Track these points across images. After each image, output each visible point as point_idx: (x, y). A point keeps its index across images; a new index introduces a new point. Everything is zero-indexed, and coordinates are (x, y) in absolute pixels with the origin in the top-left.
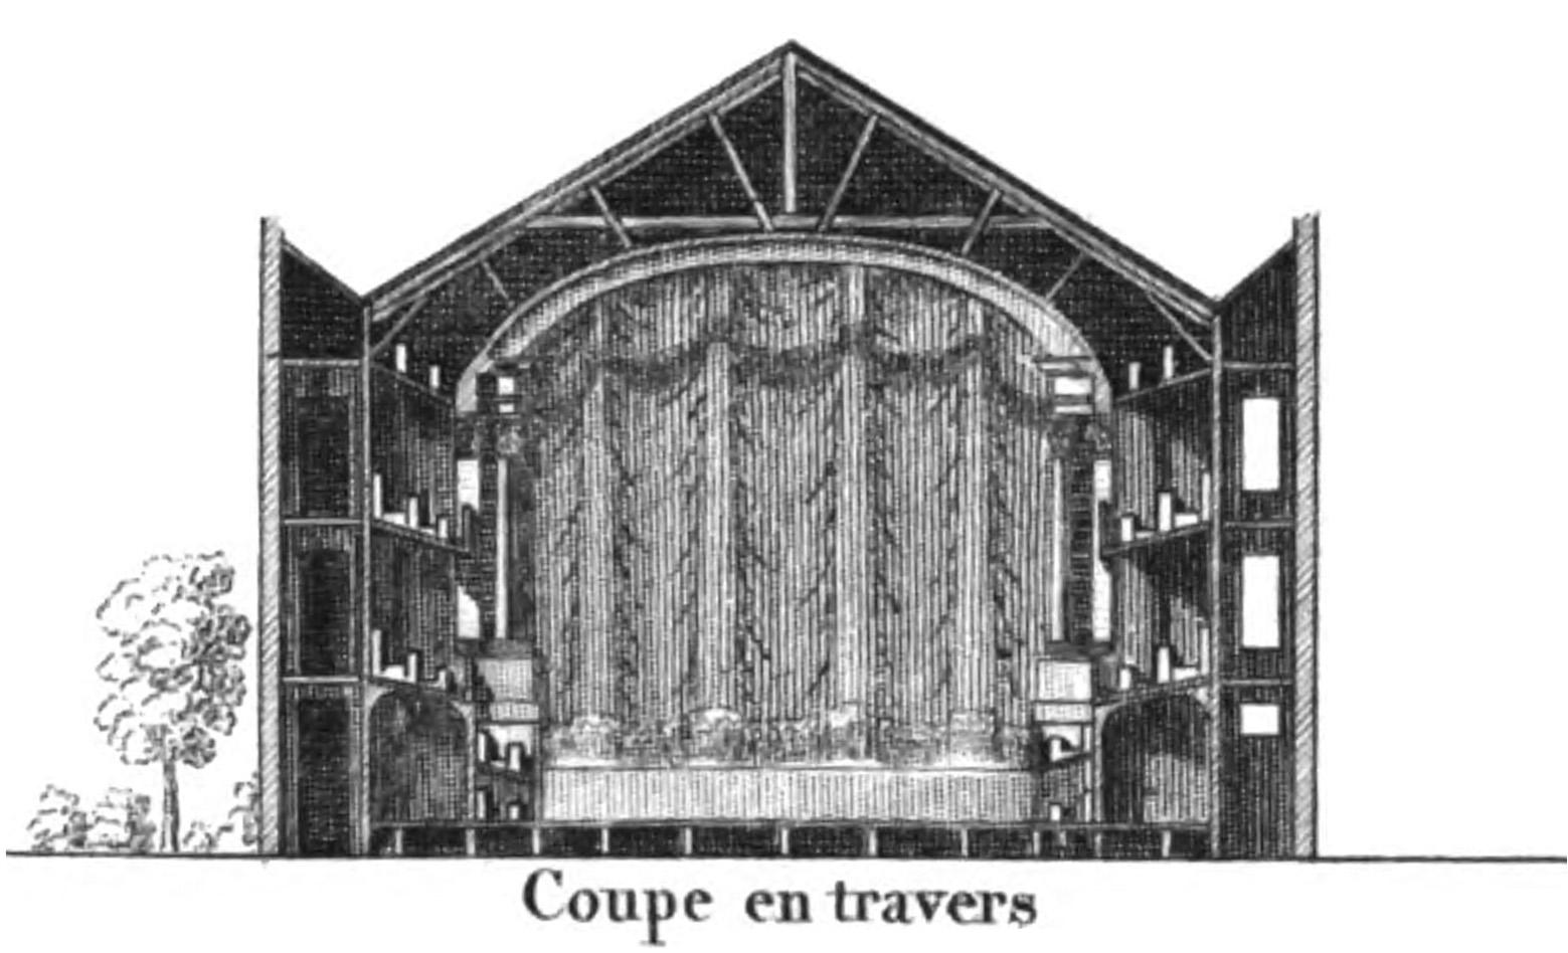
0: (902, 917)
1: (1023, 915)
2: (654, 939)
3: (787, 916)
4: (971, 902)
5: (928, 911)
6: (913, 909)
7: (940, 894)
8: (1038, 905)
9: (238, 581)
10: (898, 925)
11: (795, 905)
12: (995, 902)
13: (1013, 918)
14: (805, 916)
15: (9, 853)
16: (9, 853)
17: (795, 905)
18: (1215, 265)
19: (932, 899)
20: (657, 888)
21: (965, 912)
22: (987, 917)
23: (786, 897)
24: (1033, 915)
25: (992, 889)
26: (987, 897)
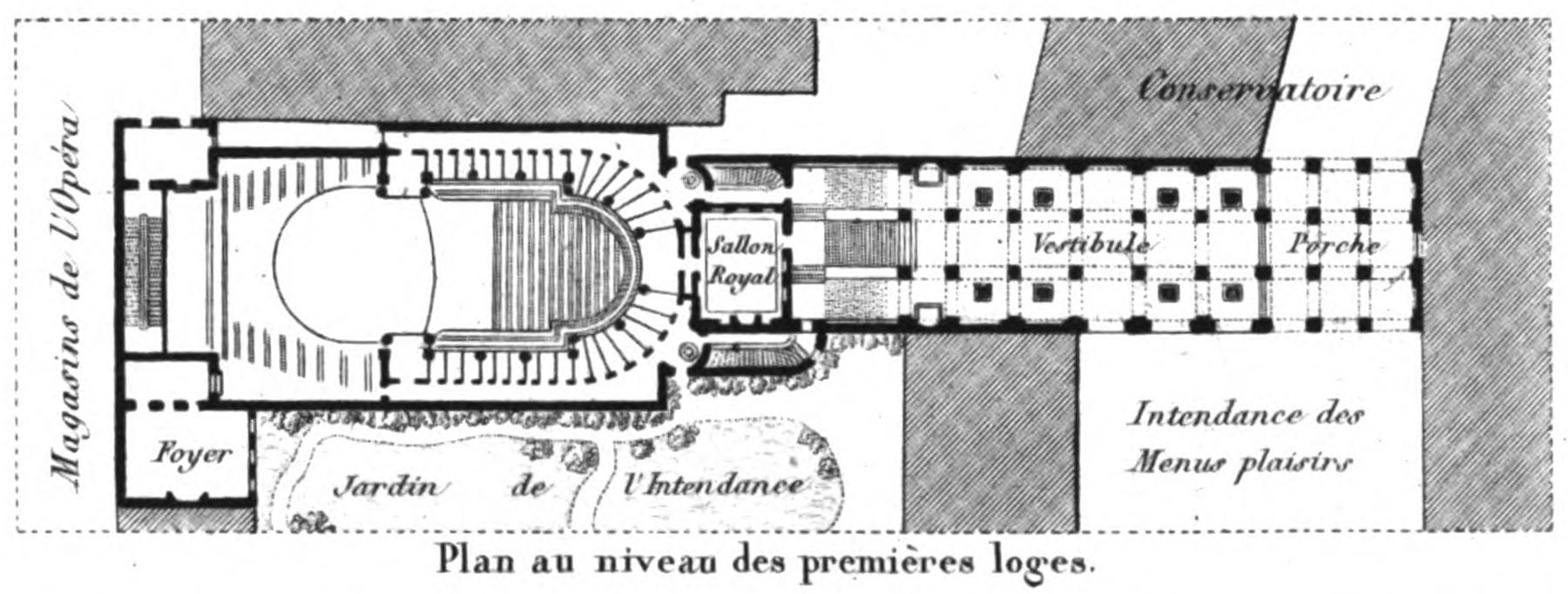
1: (1078, 568)
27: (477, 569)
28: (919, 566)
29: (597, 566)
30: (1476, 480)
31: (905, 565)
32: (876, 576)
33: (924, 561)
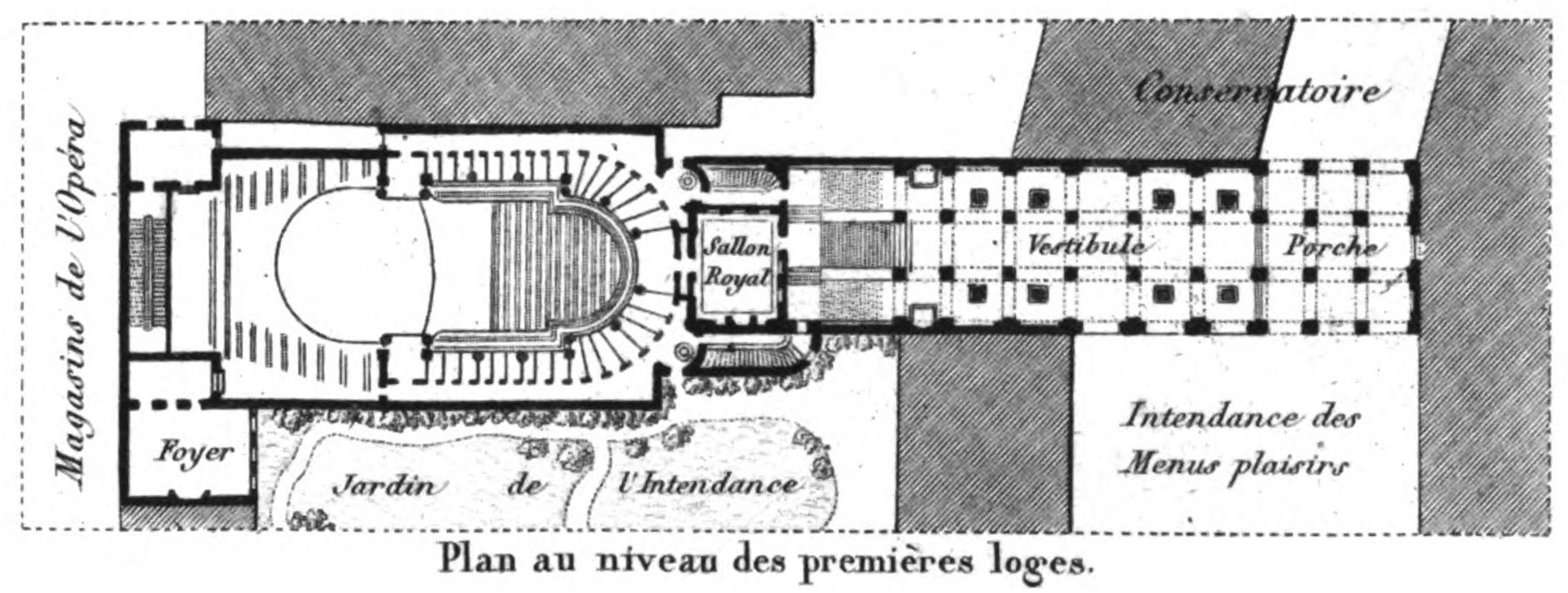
0: (547, 568)
1: (1077, 569)
2: (806, 581)
3: (862, 569)
4: (852, 561)
5: (646, 566)
6: (495, 563)
7: (652, 557)
8: (786, 562)
9: (1228, 187)
10: (544, 572)
11: (507, 561)
12: (928, 562)
13: (1072, 571)
14: (513, 568)
15: (1231, 484)
16: (1231, 484)
17: (507, 561)
18: (642, 281)
19: (647, 559)
20: (607, 552)
21: (948, 567)
22: (923, 569)
23: (862, 559)
24: (783, 567)
25: (828, 553)
26: (862, 559)
27: (479, 568)
28: (918, 566)
29: (992, 567)
30: (1471, 482)
31: (756, 563)
32: (876, 576)
33: (923, 560)
